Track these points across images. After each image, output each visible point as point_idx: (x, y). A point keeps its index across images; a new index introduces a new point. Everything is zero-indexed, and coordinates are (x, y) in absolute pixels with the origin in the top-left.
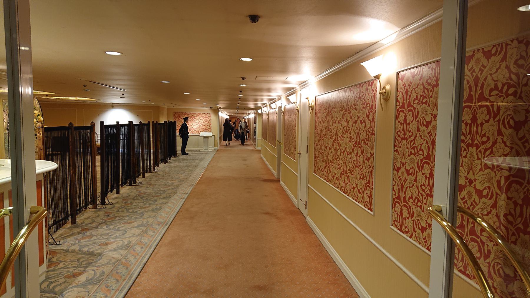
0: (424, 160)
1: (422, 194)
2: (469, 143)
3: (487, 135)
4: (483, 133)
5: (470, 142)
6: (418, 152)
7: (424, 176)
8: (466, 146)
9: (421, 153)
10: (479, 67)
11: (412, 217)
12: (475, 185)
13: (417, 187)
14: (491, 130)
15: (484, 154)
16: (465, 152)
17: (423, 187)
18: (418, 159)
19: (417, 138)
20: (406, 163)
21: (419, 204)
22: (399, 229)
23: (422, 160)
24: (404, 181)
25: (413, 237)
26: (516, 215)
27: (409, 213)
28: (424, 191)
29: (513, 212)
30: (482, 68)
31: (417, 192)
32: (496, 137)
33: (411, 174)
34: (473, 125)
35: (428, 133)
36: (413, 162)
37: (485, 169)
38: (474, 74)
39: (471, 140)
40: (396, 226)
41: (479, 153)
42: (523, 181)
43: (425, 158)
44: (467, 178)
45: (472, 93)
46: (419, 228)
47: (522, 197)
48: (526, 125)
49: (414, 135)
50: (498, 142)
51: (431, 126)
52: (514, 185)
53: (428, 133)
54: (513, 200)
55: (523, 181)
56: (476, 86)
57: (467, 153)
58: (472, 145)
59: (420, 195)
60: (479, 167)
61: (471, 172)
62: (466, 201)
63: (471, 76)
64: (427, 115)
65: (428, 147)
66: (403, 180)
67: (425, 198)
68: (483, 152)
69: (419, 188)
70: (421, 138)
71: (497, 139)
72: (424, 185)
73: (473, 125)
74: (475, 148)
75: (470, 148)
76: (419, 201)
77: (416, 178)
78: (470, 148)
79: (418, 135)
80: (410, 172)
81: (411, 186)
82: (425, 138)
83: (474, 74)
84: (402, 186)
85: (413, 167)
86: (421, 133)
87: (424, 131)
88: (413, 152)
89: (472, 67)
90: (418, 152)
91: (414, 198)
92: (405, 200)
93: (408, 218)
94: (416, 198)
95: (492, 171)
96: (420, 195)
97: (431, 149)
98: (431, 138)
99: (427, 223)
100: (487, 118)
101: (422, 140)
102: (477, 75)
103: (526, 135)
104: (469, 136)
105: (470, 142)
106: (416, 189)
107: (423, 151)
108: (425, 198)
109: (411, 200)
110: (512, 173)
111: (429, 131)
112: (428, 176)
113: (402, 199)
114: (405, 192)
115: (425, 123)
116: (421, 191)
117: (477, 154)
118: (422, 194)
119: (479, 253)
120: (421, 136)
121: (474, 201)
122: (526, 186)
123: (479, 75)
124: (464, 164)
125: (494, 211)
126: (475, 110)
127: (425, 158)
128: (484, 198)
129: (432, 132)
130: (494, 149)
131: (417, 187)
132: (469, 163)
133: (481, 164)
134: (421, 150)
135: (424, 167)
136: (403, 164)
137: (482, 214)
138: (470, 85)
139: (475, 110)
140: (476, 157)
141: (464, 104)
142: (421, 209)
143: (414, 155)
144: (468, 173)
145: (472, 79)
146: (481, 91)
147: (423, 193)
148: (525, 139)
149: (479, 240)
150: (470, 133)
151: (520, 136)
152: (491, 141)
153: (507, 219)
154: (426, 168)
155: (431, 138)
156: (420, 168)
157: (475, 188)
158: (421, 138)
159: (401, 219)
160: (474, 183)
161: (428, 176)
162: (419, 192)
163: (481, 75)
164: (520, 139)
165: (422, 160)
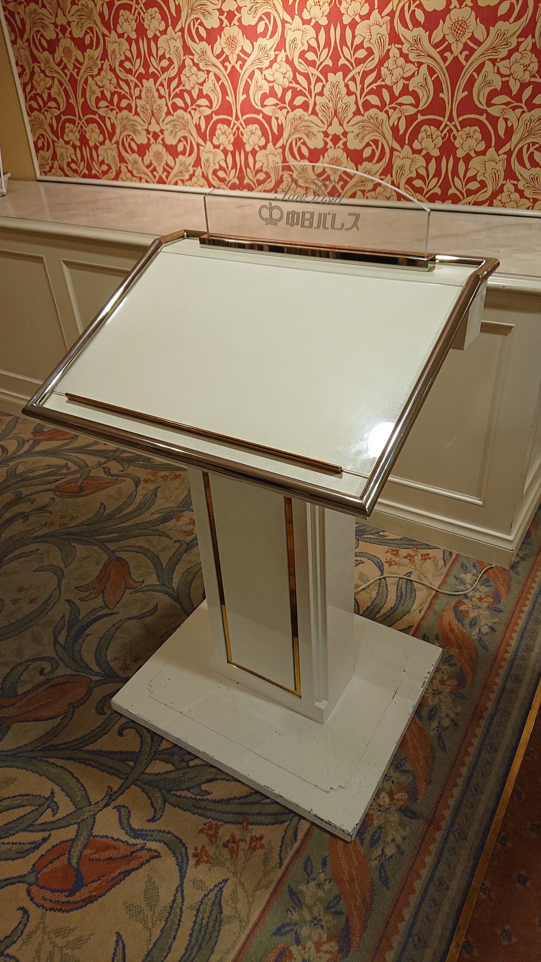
0: (63, 118)
1: (127, 82)
2: (141, 73)
3: (167, 56)
4: (160, 53)
5: (142, 70)
6: (45, 104)
7: (123, 41)
8: (137, 78)
9: (52, 104)
10: (464, 40)
11: (111, 135)
12: (163, 140)
13: (113, 70)
14: (172, 47)
15: (169, 87)
16: (137, 89)
17: (73, 166)
18: (49, 116)
19: (36, 77)
20: (69, 23)
21: (124, 103)
22: (85, 176)
23: (58, 118)
24: (75, 67)
25: (122, 175)
26: (228, 167)
27: (102, 132)
28: (129, 71)
29: (223, 164)
31: (114, 81)
32: (183, 58)
33: (90, 46)
35: (59, 65)
36: (89, 17)
37: (175, 111)
38: (227, 64)
39: (87, 168)
40: (75, 171)
41: (160, 88)
43: (64, 113)
44: (148, 132)
46: (133, 151)
47: (232, 140)
49: (28, 71)
50: (186, 64)
51: (61, 49)
52: (219, 125)
53: (59, 65)
54: (222, 147)
57: (141, 91)
58: (147, 76)
59: (122, 84)
60: (165, 109)
61: (153, 120)
62: (227, 56)
64: (44, 26)
65: (65, 91)
66: (70, 67)
67: (136, 86)
68: (165, 84)
69: (118, 69)
70: (46, 76)
71: (184, 60)
72: (127, 59)
74: (151, 80)
75: (144, 81)
76: (122, 97)
77: (105, 50)
78: (144, 81)
79: (37, 69)
80: (87, 41)
81: (96, 71)
82: (55, 75)
83: (227, 64)
84: (73, 81)
85: (91, 29)
86: (42, 65)
87: (47, 61)
88: (35, 105)
90: (45, 104)
91: (109, 97)
92: (86, 109)
93: (103, 143)
94: (113, 94)
95: (186, 111)
96: (122, 84)
97: (71, 94)
98: (66, 74)
99: (148, 132)
100: (162, 27)
101: (49, 81)
103: (153, 162)
104: (139, 60)
105: (142, 70)
106: (111, 75)
107: (55, 100)
108: (136, 86)
109: (103, 104)
111: (58, 60)
112: (78, 143)
113: (78, 110)
114: (84, 91)
115: (45, 44)
116: (123, 75)
117: (158, 90)
118: (127, 82)
119: (263, 138)
120: (43, 72)
121: (167, 164)
124: (138, 109)
125: (199, 171)
127: (64, 113)
128: (180, 157)
129: (65, 60)
130: (183, 77)
131: (113, 70)
132: (148, 107)
133: (167, 105)
134: (50, 98)
135: (67, 130)
136: (63, 29)
137: (183, 181)
138: (65, 88)
140: (156, 95)
142: (130, 111)
143: (40, 111)
144: (150, 123)
145: (226, 74)
146: (83, 99)
147: (130, 77)
148: (446, 43)
149: (260, 117)
150: (83, 159)
152: (176, 65)
153: (218, 177)
154: (71, 131)
155: (66, 74)
156: (59, 133)
157: (164, 144)
158: (46, 76)
159: (143, 46)
160: (162, 136)
161: (78, 143)
162: (118, 77)
164: (436, 46)
165: (58, 118)
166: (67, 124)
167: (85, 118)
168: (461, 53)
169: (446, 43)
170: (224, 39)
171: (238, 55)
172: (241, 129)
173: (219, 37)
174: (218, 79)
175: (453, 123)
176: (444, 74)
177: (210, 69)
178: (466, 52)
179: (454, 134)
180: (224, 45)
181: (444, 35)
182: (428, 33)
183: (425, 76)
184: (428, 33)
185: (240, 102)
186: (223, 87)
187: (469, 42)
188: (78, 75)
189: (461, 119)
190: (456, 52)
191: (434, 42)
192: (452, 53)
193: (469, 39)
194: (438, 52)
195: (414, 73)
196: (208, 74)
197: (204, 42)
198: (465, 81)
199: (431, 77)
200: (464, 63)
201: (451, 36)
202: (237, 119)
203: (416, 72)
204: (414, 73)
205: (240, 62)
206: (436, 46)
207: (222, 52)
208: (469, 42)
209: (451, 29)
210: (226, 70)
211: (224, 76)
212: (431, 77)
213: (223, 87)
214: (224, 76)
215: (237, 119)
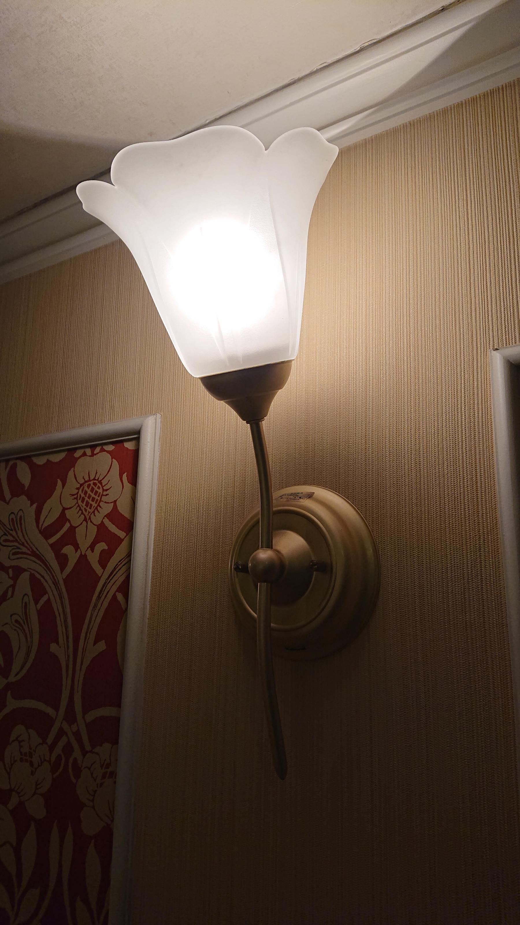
10: (97, 519)
30: (112, 528)
34: (55, 833)
38: (68, 550)
42: (50, 711)
45: (53, 647)
48: (71, 474)
55: (50, 711)
56: (78, 618)
63: (54, 564)
73: (55, 833)
83: (68, 550)
89: (62, 519)
102: (83, 558)
103: (68, 514)
110: (12, 679)
122: (61, 733)
123: (94, 559)
126: (68, 749)
139: (68, 749)
141: (12, 704)
145: (60, 577)
148: (67, 525)
151: (49, 517)
163: (103, 562)
164: (47, 533)
166: (19, 729)
167: (91, 716)
168: (92, 547)
169: (67, 525)
170: (72, 485)
171: (101, 527)
172: (77, 753)
173: (59, 483)
174: (37, 588)
175: (74, 728)
176: (61, 598)
177: (23, 563)
178: (102, 546)
179: (75, 759)
180: (69, 502)
181: (64, 509)
182: (35, 506)
183: (26, 599)
184: (35, 506)
185: (86, 663)
186: (47, 615)
187: (107, 522)
188: (103, 564)
189: (91, 716)
190: (84, 543)
191: (45, 525)
192: (77, 547)
193: (108, 516)
194: (51, 546)
195: (6, 592)
196: (15, 578)
197: (24, 498)
198: (101, 614)
199: (36, 603)
200: (98, 570)
201: (74, 510)
202: (70, 717)
203: (10, 589)
204: (6, 592)
205: (102, 546)
206: (47, 533)
207: (62, 519)
208: (107, 522)
209: (75, 496)
210: (63, 566)
211: (56, 583)
212: (36, 603)
213: (47, 615)
214: (56, 583)
215: (70, 717)
